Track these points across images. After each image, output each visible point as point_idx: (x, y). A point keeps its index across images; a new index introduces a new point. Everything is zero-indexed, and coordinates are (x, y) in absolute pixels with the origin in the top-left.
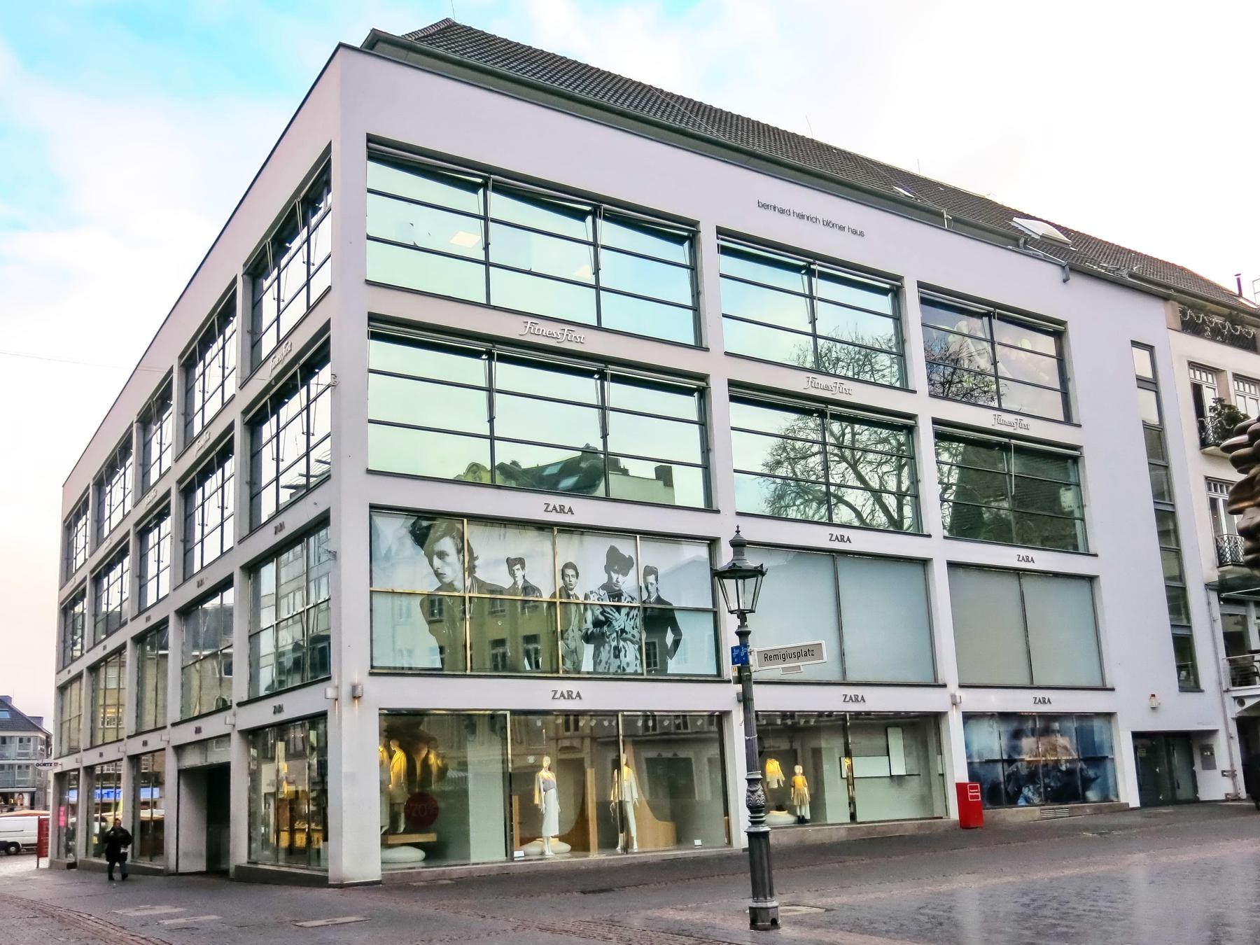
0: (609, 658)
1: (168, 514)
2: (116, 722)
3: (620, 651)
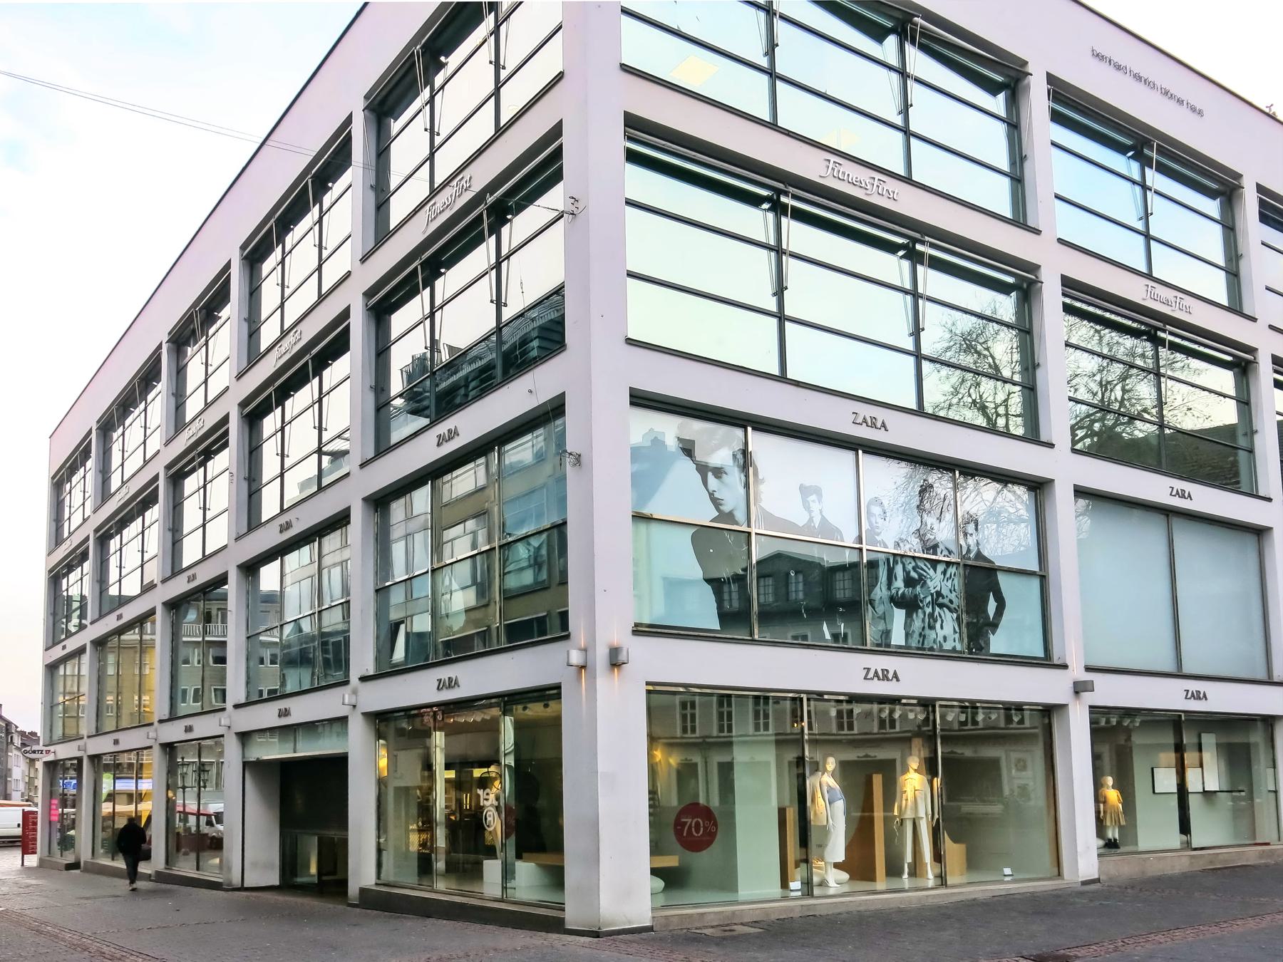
0: (923, 628)
1: (226, 445)
2: (115, 711)
3: (935, 621)
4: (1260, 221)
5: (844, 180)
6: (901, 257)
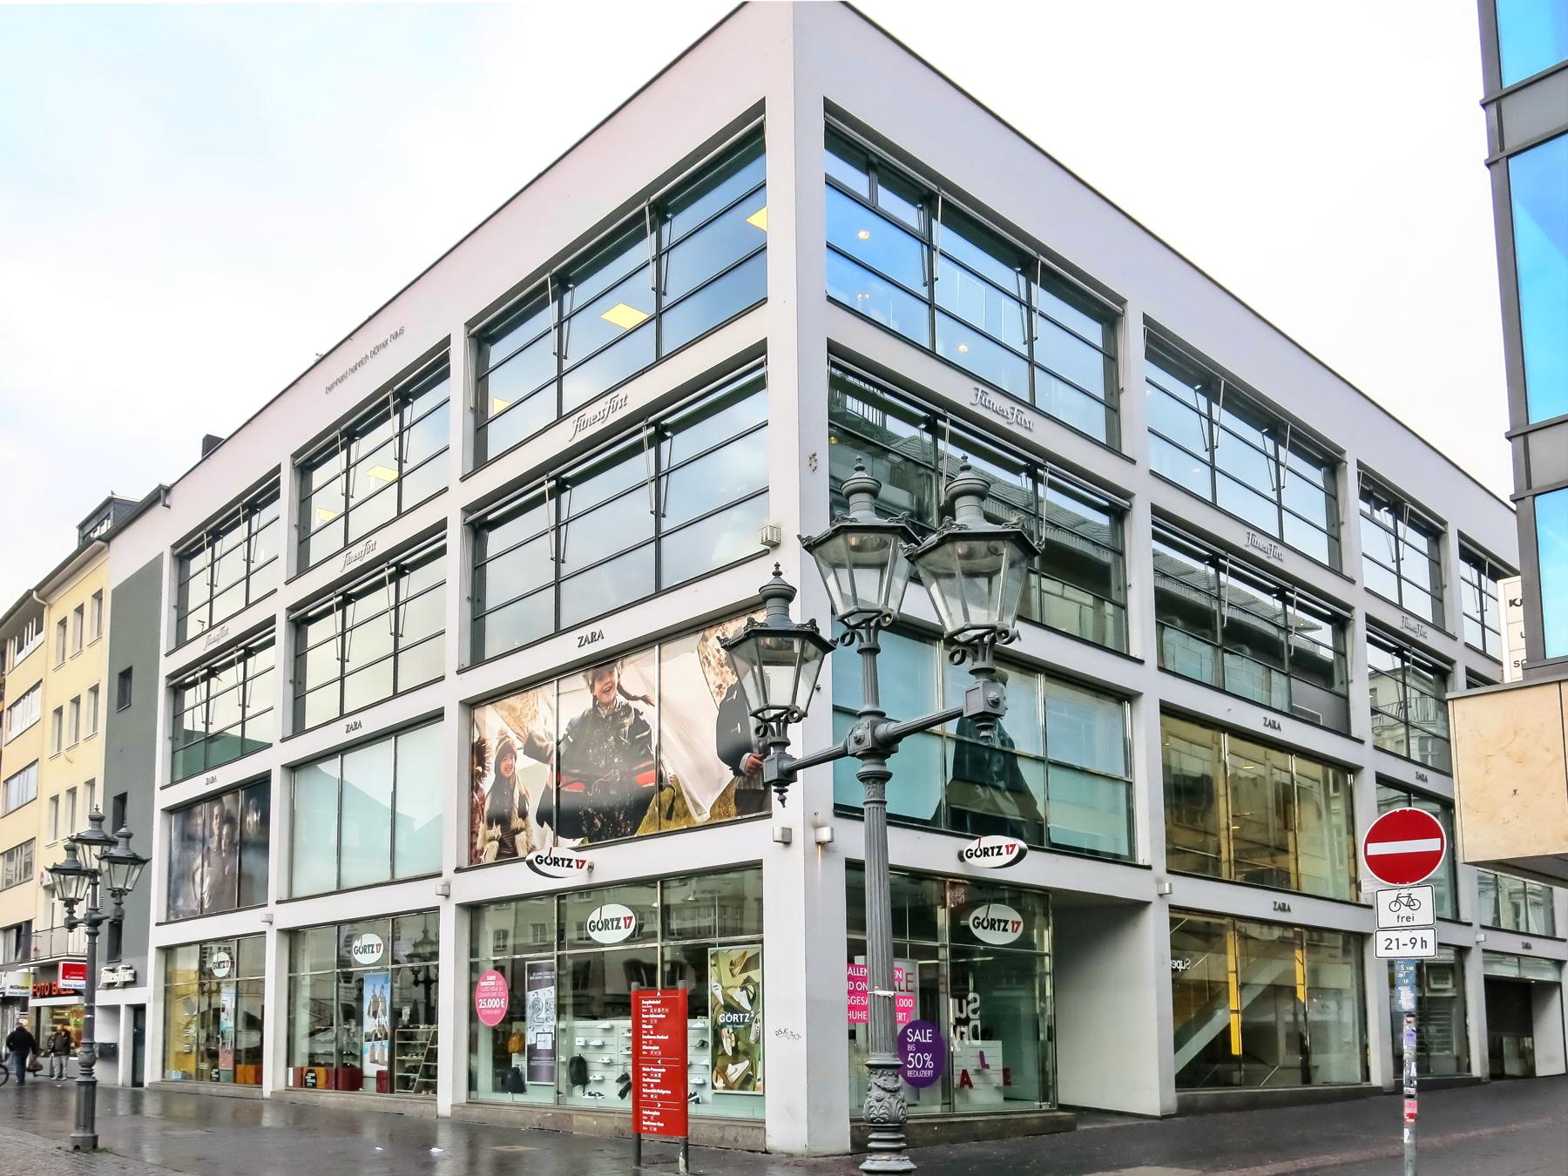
4: (1146, 358)
5: (989, 408)
6: (924, 430)
